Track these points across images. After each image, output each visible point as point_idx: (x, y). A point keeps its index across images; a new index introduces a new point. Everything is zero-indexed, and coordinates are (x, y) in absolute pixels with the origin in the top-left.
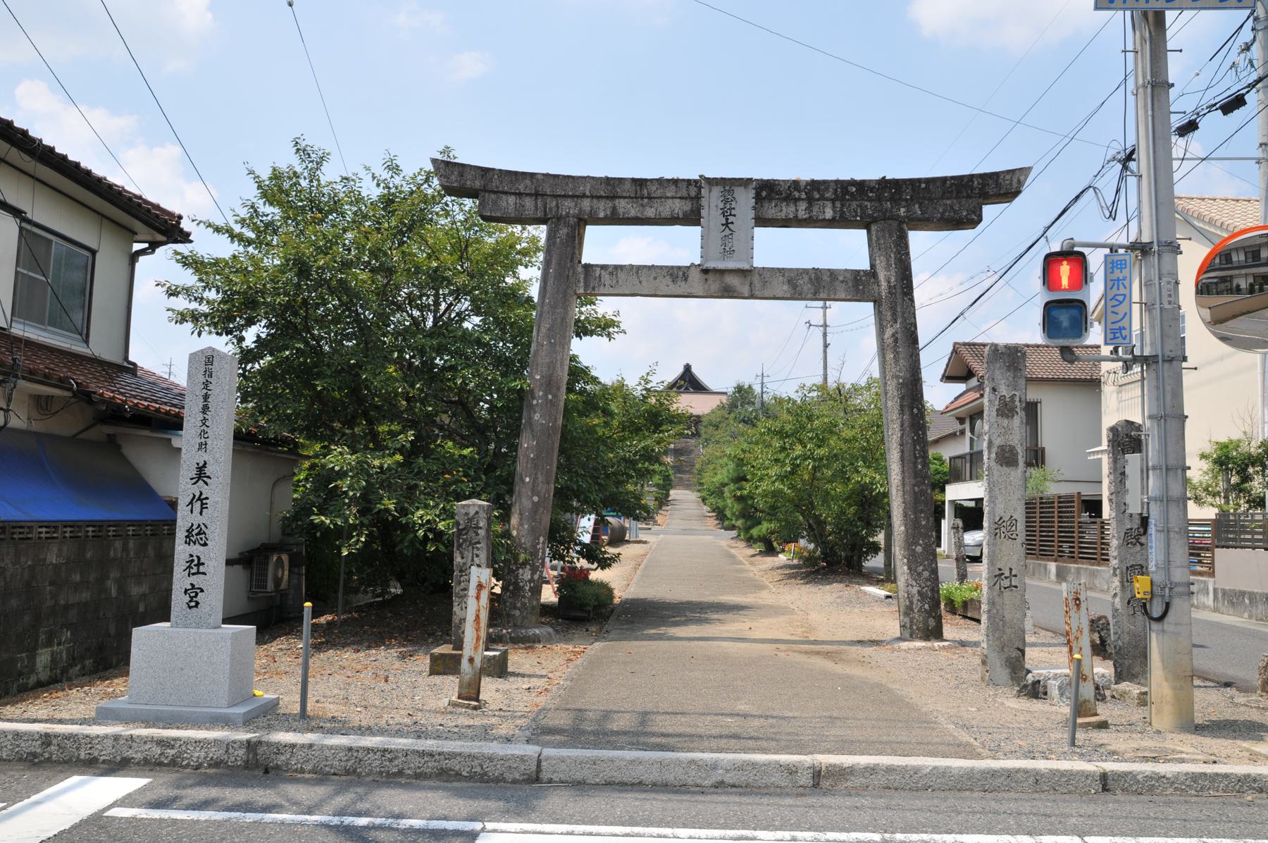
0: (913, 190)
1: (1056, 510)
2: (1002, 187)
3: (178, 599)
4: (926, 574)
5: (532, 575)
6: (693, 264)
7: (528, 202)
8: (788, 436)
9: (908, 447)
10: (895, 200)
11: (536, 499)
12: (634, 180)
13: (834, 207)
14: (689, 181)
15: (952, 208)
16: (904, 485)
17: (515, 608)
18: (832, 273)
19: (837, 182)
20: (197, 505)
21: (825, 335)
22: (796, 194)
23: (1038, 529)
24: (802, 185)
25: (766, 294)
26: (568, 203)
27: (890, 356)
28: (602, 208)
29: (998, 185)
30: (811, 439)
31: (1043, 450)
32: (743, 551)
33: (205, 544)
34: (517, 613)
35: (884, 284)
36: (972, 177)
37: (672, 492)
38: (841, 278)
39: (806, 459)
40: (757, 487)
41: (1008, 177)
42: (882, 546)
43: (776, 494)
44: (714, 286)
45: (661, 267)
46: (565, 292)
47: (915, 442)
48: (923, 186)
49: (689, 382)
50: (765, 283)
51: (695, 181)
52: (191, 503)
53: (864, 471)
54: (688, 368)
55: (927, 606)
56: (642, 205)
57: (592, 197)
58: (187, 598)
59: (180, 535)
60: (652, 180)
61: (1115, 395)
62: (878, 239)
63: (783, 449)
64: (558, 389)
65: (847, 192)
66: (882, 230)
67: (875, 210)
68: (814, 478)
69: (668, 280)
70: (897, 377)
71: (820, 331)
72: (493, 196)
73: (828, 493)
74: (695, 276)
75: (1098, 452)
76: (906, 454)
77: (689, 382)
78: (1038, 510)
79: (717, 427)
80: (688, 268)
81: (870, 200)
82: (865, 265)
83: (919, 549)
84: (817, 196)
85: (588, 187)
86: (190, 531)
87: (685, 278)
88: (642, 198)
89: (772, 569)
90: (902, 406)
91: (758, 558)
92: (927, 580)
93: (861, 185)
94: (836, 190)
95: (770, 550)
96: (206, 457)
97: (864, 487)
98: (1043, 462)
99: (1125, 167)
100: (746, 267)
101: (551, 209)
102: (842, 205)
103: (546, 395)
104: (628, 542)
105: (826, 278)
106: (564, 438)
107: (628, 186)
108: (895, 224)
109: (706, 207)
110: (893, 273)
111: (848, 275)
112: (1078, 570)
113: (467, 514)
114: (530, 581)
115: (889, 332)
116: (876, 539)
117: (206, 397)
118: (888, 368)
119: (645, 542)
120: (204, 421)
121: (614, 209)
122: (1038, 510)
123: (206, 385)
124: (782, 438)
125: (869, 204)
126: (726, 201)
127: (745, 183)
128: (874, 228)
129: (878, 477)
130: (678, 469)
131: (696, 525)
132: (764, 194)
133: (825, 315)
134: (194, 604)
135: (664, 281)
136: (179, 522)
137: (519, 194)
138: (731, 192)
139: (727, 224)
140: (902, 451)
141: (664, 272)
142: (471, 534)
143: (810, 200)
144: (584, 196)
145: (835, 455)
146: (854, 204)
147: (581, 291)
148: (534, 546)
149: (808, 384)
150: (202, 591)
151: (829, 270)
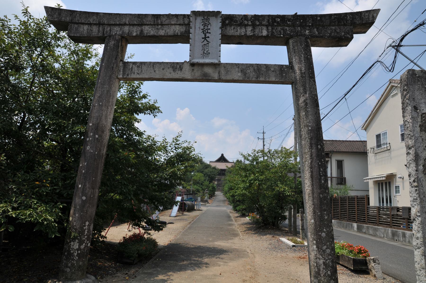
0: (313, 20)
1: (356, 202)
2: (362, 21)
4: (328, 251)
5: (79, 246)
6: (185, 61)
7: (95, 29)
8: (248, 171)
9: (316, 169)
10: (303, 26)
11: (84, 198)
12: (153, 15)
13: (268, 30)
14: (184, 15)
15: (335, 31)
16: (313, 193)
17: (67, 267)
18: (267, 67)
19: (269, 16)
21: (264, 142)
22: (246, 22)
23: (347, 209)
25: (228, 78)
27: (303, 113)
28: (135, 30)
29: (361, 19)
30: (258, 172)
31: (345, 178)
32: (234, 215)
34: (68, 270)
35: (298, 72)
36: (346, 14)
37: (216, 192)
38: (272, 69)
39: (255, 180)
40: (236, 192)
41: (367, 14)
42: (288, 217)
43: (243, 195)
44: (198, 73)
45: (167, 63)
46: (110, 77)
47: (319, 166)
49: (222, 159)
50: (227, 72)
51: (188, 15)
53: (281, 185)
54: (222, 155)
55: (329, 273)
56: (158, 29)
57: (130, 25)
60: (163, 15)
61: (374, 157)
62: (294, 47)
63: (246, 176)
64: (103, 132)
65: (275, 21)
66: (296, 42)
67: (291, 31)
68: (259, 188)
69: (171, 70)
70: (308, 126)
71: (262, 141)
72: (76, 26)
73: (265, 195)
74: (187, 68)
75: (367, 179)
76: (315, 174)
77: (222, 159)
78: (347, 202)
79: (231, 173)
80: (183, 63)
81: (288, 26)
82: (286, 62)
83: (324, 235)
84: (258, 23)
85: (128, 19)
87: (181, 69)
88: (158, 25)
89: (243, 224)
90: (311, 144)
91: (239, 218)
92: (329, 255)
93: (283, 18)
94: (269, 20)
95: (244, 215)
97: (279, 193)
98: (345, 182)
99: (397, 51)
100: (216, 61)
101: (107, 32)
102: (272, 29)
103: (94, 135)
104: (195, 210)
105: (264, 69)
106: (107, 164)
107: (150, 18)
108: (303, 38)
109: (193, 28)
110: (303, 65)
111: (277, 68)
112: (368, 228)
114: (78, 250)
115: (302, 99)
116: (285, 214)
118: (302, 121)
119: (201, 210)
121: (142, 31)
122: (347, 202)
124: (245, 171)
125: (288, 28)
126: (205, 25)
127: (216, 14)
128: (291, 41)
129: (287, 188)
130: (218, 185)
131: (221, 204)
132: (227, 22)
133: (264, 135)
135: (168, 71)
137: (90, 24)
138: (208, 19)
139: (205, 38)
140: (312, 172)
143: (254, 26)
144: (125, 24)
145: (268, 179)
146: (279, 28)
147: (121, 76)
148: (82, 228)
149: (257, 150)
151: (265, 65)
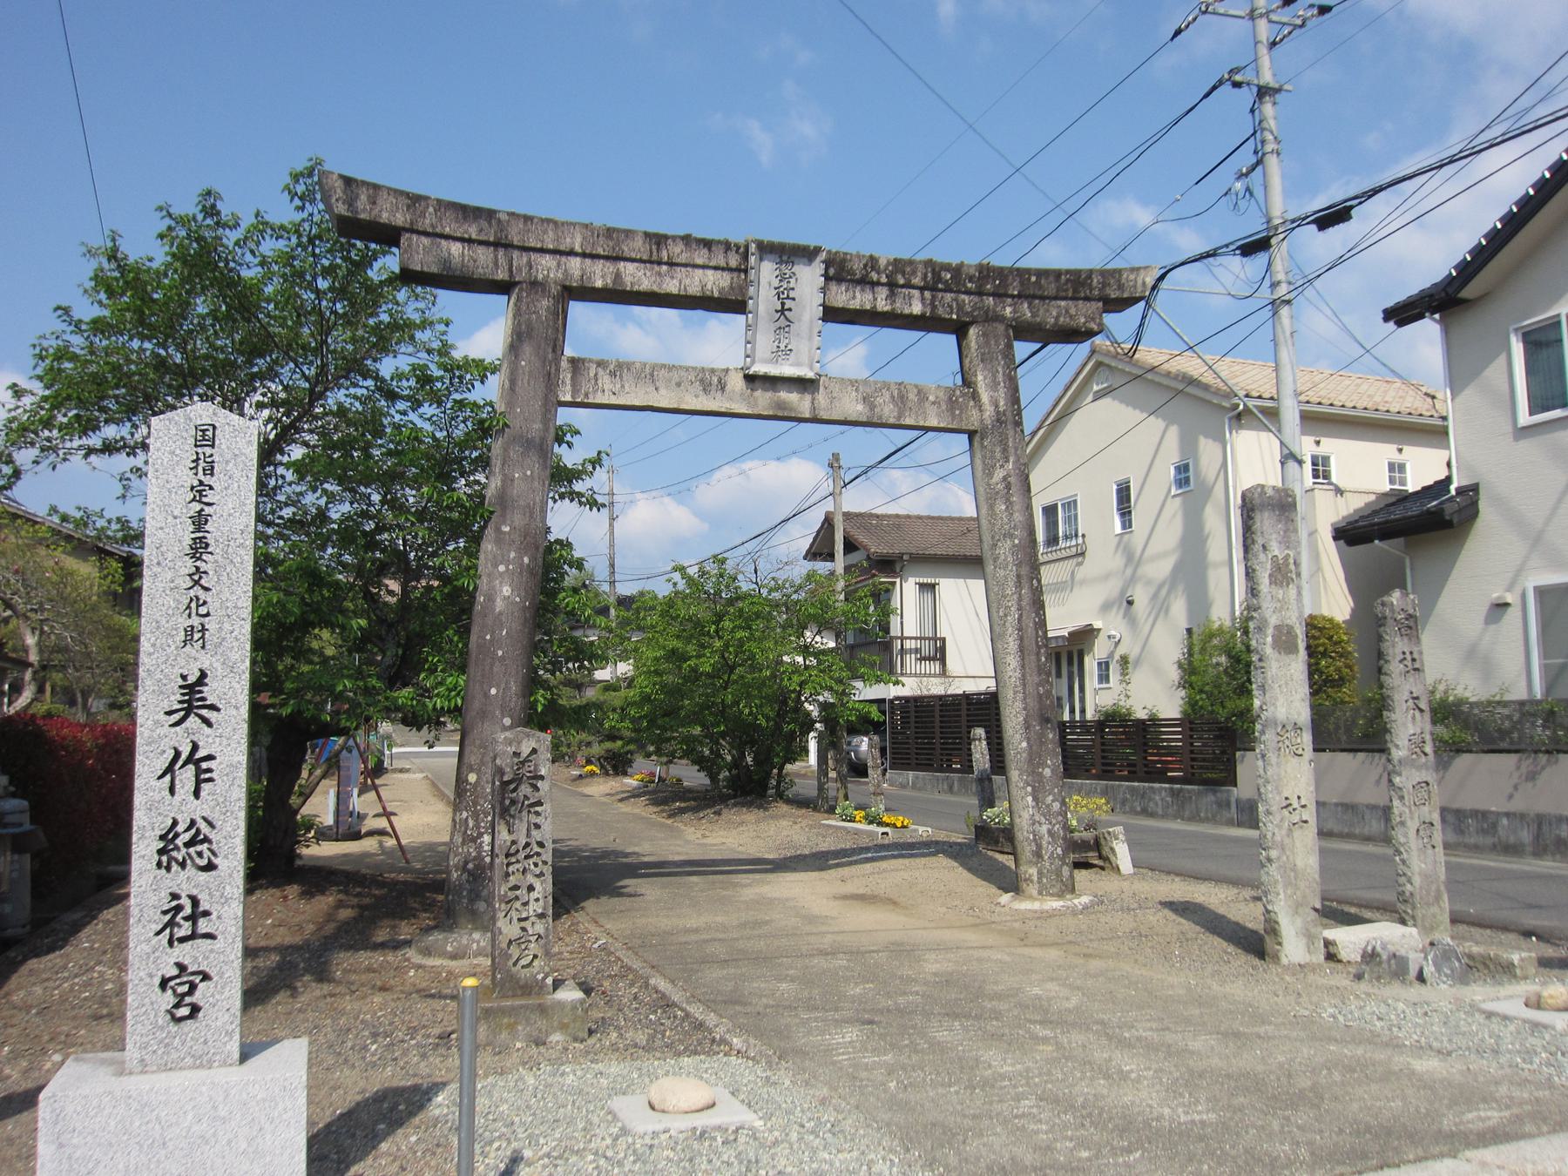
0: (1022, 283)
3: (145, 1003)
13: (923, 299)
20: (186, 776)
22: (874, 276)
24: (882, 262)
26: (547, 261)
33: (210, 867)
41: (1132, 277)
48: (1033, 279)
52: (170, 769)
55: (1059, 851)
56: (659, 274)
57: (584, 255)
58: (169, 999)
59: (144, 848)
72: (425, 241)
86: (169, 837)
88: (660, 263)
94: (925, 276)
96: (205, 661)
113: (517, 754)
117: (200, 521)
120: (197, 577)
123: (200, 492)
126: (782, 278)
134: (186, 1010)
136: (140, 818)
139: (782, 311)
140: (1021, 639)
141: (692, 377)
142: (525, 789)
143: (892, 285)
146: (949, 297)
150: (206, 977)
